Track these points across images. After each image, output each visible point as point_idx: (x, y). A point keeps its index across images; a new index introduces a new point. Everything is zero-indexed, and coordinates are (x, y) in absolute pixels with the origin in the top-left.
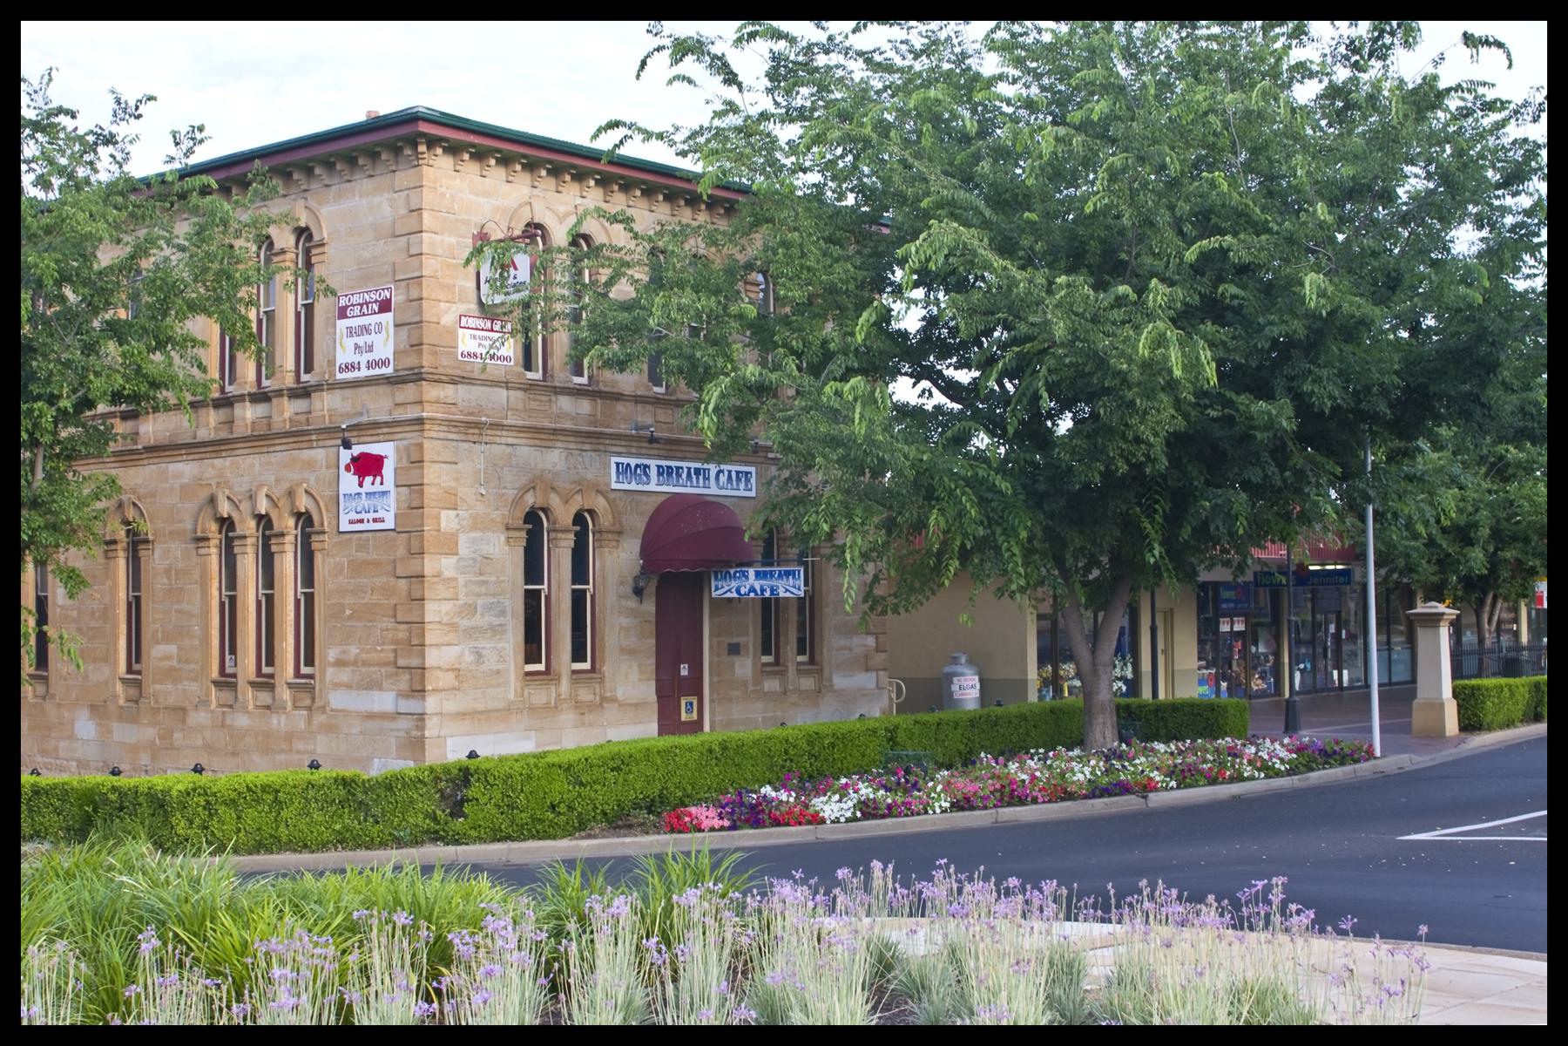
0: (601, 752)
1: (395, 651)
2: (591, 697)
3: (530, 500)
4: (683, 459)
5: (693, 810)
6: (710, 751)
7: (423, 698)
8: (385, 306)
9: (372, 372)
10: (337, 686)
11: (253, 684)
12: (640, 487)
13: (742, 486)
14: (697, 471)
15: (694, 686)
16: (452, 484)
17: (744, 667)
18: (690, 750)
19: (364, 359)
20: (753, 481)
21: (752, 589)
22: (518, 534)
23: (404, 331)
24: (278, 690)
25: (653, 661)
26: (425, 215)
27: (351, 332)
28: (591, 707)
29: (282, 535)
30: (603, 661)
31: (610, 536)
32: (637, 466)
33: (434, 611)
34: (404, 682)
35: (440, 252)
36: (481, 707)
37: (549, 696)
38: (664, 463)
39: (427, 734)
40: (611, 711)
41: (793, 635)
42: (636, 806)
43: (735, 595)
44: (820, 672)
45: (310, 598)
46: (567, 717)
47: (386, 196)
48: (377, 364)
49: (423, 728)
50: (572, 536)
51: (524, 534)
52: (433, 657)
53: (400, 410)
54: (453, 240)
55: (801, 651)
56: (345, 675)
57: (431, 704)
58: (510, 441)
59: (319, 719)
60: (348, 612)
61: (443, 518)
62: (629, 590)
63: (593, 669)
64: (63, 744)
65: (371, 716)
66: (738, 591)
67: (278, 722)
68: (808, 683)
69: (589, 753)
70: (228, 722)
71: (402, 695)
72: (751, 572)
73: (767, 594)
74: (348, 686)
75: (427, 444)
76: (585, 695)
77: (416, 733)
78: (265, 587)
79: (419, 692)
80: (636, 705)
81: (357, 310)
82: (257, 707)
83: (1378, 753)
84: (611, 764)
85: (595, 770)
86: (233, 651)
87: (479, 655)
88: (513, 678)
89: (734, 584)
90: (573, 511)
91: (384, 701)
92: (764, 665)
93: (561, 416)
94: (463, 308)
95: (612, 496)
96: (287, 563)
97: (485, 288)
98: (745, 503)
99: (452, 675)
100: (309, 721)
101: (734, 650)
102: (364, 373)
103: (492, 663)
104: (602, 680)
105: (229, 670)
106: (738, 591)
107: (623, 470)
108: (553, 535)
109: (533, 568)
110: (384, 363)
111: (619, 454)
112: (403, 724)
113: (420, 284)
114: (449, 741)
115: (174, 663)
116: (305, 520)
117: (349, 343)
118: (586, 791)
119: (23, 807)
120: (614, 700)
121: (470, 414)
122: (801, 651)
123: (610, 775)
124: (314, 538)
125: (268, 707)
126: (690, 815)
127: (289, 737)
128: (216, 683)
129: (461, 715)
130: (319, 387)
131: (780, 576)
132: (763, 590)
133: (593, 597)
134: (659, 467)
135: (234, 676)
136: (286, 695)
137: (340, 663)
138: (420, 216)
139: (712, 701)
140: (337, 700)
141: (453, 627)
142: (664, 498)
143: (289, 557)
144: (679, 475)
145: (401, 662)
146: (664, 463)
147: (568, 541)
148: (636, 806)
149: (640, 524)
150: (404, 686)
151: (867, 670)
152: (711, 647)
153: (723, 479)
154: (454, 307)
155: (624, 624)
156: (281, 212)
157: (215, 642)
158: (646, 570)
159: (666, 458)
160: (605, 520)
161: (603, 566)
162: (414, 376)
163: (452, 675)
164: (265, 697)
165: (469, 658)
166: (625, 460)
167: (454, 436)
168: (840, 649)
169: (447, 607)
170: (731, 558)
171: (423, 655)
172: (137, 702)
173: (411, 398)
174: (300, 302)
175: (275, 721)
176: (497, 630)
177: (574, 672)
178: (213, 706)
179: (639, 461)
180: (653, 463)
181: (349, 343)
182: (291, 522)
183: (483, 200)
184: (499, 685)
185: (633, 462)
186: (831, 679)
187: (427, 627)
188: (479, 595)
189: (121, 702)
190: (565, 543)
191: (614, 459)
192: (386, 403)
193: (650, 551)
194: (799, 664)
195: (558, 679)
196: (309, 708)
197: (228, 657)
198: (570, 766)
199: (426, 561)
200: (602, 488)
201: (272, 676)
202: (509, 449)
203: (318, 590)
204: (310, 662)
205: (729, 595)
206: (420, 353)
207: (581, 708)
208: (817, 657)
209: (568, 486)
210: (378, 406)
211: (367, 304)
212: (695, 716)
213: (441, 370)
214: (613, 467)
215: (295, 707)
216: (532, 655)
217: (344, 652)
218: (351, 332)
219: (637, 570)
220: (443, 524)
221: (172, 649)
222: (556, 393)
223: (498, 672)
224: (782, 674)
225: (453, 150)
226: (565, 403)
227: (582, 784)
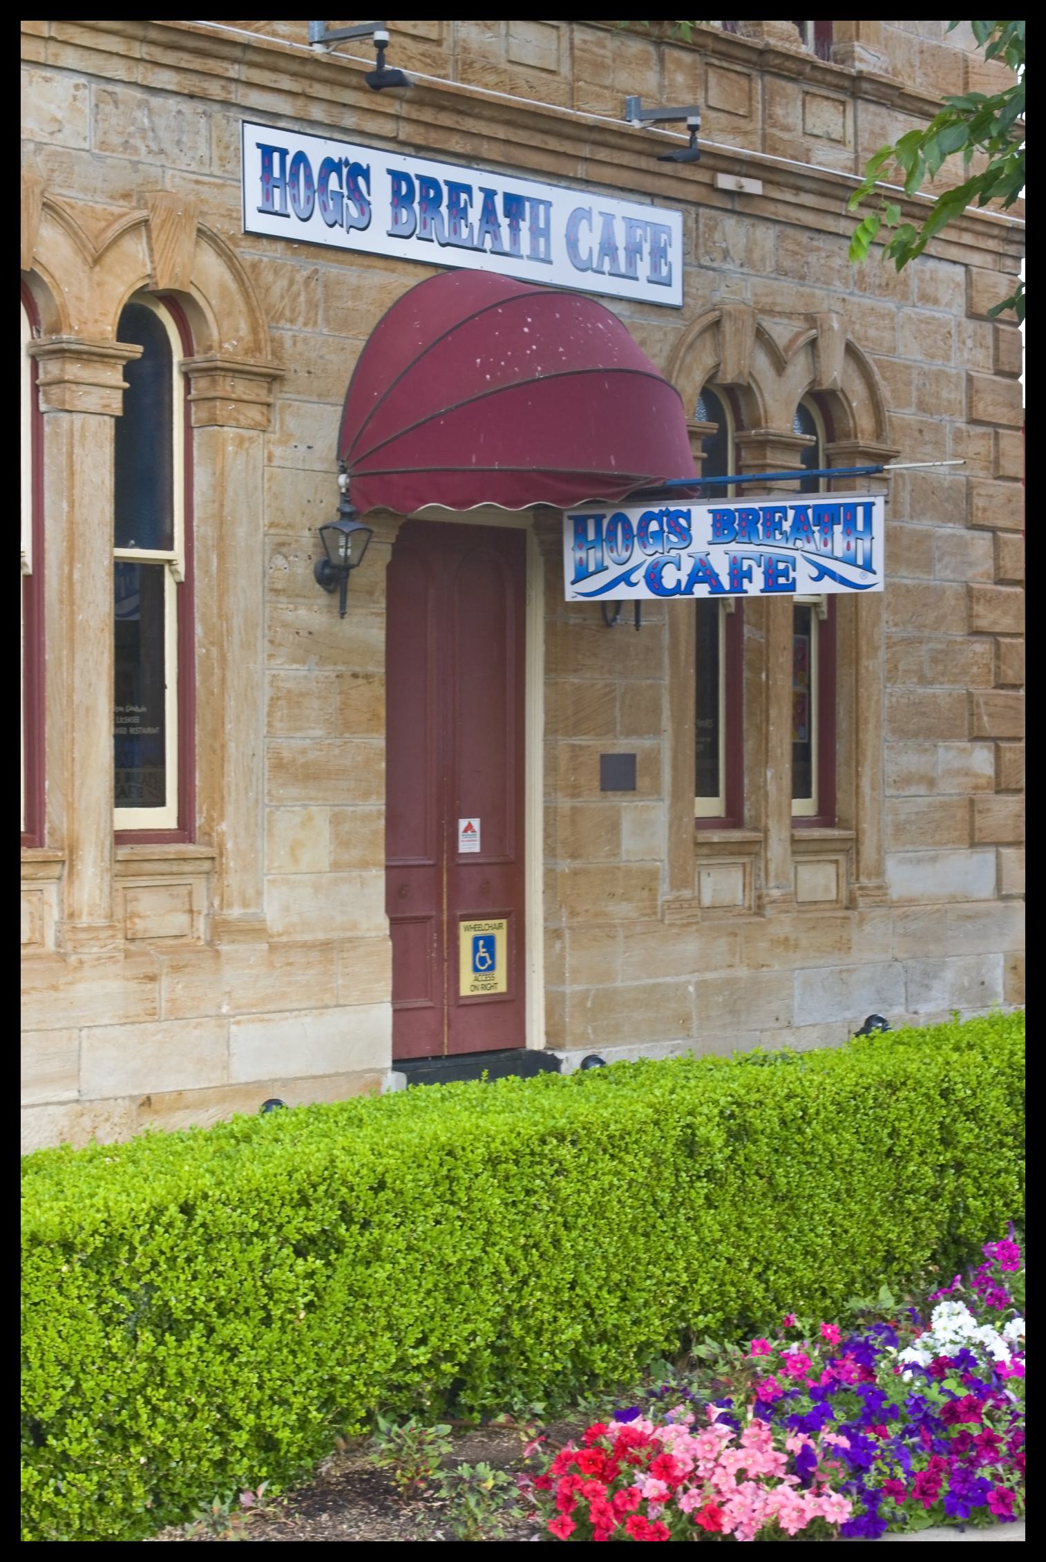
0: (253, 1172)
2: (179, 921)
4: (470, 160)
5: (676, 1440)
6: (690, 1146)
12: (337, 237)
13: (644, 268)
14: (514, 204)
15: (501, 889)
17: (647, 828)
18: (615, 1146)
21: (703, 572)
25: (377, 804)
28: (181, 955)
30: (218, 802)
31: (241, 388)
32: (330, 166)
38: (415, 166)
40: (243, 968)
41: (781, 738)
42: (400, 1405)
43: (642, 592)
44: (852, 848)
50: (115, 376)
55: (800, 789)
62: (304, 570)
63: (185, 830)
66: (654, 580)
68: (819, 880)
69: (195, 1176)
72: (701, 515)
76: (158, 913)
80: (326, 946)
84: (299, 1224)
85: (227, 1253)
89: (640, 556)
90: (119, 292)
92: (703, 823)
95: (248, 253)
98: (654, 320)
101: (620, 774)
104: (214, 865)
106: (654, 580)
107: (282, 170)
108: (51, 369)
111: (271, 119)
118: (185, 1354)
119: (745, 708)
120: (254, 931)
122: (800, 789)
123: (292, 1273)
126: (663, 1467)
131: (801, 526)
132: (739, 575)
133: (185, 590)
134: (398, 177)
139: (553, 934)
142: (409, 280)
144: (458, 212)
146: (415, 166)
147: (100, 393)
148: (400, 1405)
149: (328, 352)
151: (973, 844)
152: (551, 767)
158: (356, 507)
160: (226, 333)
161: (220, 485)
168: (906, 780)
170: (627, 489)
177: (122, 838)
179: (338, 151)
180: (380, 162)
185: (318, 150)
186: (879, 872)
190: (92, 399)
191: (256, 134)
193: (370, 444)
194: (797, 822)
198: (114, 1242)
200: (216, 224)
205: (621, 593)
208: (843, 806)
209: (102, 205)
212: (500, 981)
214: (254, 159)
219: (328, 507)
227: (166, 1323)
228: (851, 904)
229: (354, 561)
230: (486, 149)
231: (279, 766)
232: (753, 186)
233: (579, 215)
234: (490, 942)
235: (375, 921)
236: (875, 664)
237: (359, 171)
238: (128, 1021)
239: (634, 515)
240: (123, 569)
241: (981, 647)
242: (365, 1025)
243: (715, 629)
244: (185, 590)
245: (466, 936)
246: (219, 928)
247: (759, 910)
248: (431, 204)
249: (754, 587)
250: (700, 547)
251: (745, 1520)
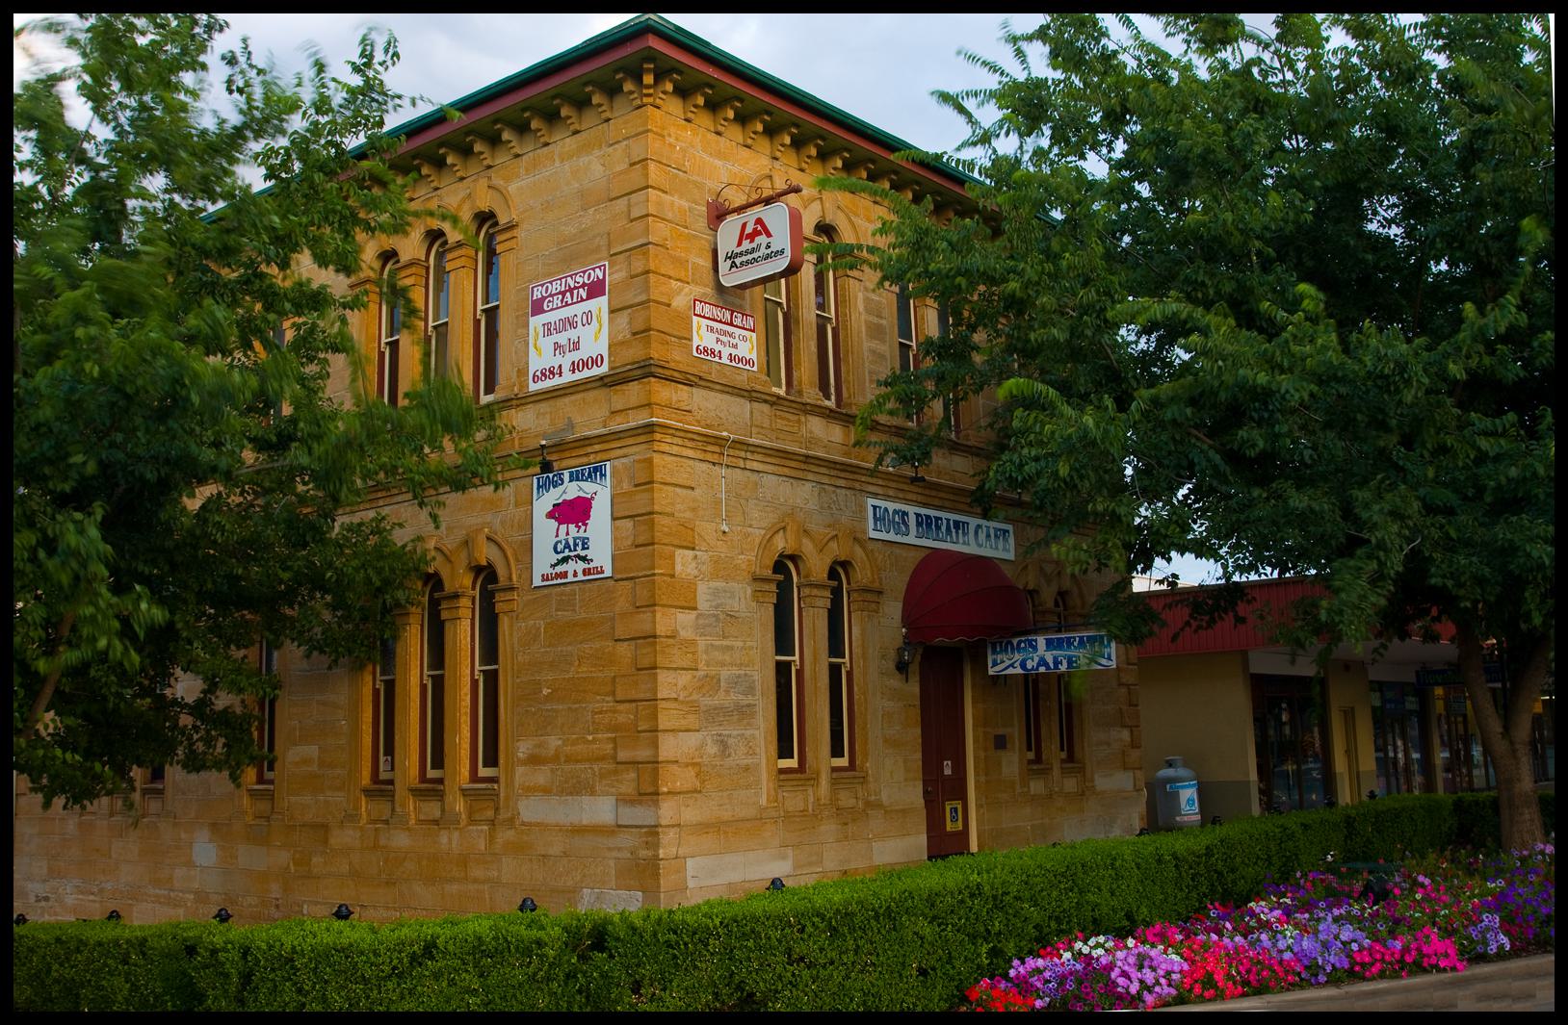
1: (614, 740)
3: (780, 544)
7: (656, 804)
8: (595, 290)
9: (578, 376)
10: (530, 791)
11: (414, 791)
12: (899, 539)
14: (957, 524)
16: (688, 515)
19: (565, 362)
20: (1011, 540)
21: (1043, 662)
22: (766, 587)
23: (623, 319)
24: (449, 798)
25: (919, 755)
26: (652, 166)
27: (549, 329)
29: (456, 596)
32: (895, 512)
33: (669, 684)
34: (628, 783)
35: (670, 216)
36: (726, 815)
37: (806, 801)
38: (924, 511)
39: (661, 853)
44: (1082, 770)
45: (492, 679)
46: (828, 828)
47: (597, 152)
48: (585, 364)
49: (656, 846)
51: (773, 587)
52: (670, 747)
53: (619, 418)
54: (685, 204)
55: (837, 752)
56: (541, 776)
57: (667, 811)
58: (756, 466)
59: (505, 835)
60: (545, 691)
61: (678, 560)
62: (892, 666)
64: (180, 872)
65: (579, 830)
66: (1023, 665)
67: (448, 841)
68: (1071, 784)
70: (382, 842)
71: (623, 800)
72: (1041, 641)
73: (1063, 668)
74: (546, 791)
75: (657, 459)
76: (846, 799)
77: (644, 853)
78: (431, 667)
79: (649, 795)
80: (903, 811)
81: (557, 301)
82: (420, 822)
83: (974, 847)
86: (390, 750)
87: (723, 744)
88: (764, 776)
89: (1018, 657)
90: (828, 561)
91: (600, 809)
93: (812, 441)
94: (697, 290)
95: (871, 546)
96: (463, 633)
97: (724, 266)
99: (691, 772)
100: (491, 838)
101: (1001, 743)
102: (568, 377)
103: (739, 757)
105: (383, 776)
106: (1023, 665)
108: (806, 591)
109: (783, 640)
110: (595, 362)
111: (875, 495)
112: (626, 840)
113: (646, 254)
114: (690, 862)
115: (315, 768)
116: (486, 574)
117: (546, 344)
120: (878, 805)
121: (708, 426)
122: (837, 752)
124: (499, 597)
125: (436, 822)
127: (464, 861)
128: (367, 792)
129: (704, 828)
130: (506, 403)
132: (1057, 663)
133: (849, 674)
134: (918, 515)
135: (391, 782)
136: (460, 806)
137: (534, 760)
138: (646, 168)
139: (979, 806)
140: (530, 810)
141: (694, 707)
142: (922, 554)
143: (466, 624)
144: (938, 528)
145: (622, 755)
146: (924, 511)
147: (824, 600)
149: (897, 582)
150: (627, 787)
152: (975, 741)
153: (982, 536)
154: (687, 288)
155: (887, 706)
156: (457, 195)
157: (367, 740)
158: (908, 641)
159: (925, 505)
162: (646, 371)
163: (691, 772)
164: (432, 809)
165: (712, 749)
166: (882, 504)
167: (690, 453)
169: (684, 678)
171: (655, 745)
172: (268, 819)
173: (634, 401)
174: (480, 307)
175: (444, 840)
176: (744, 713)
178: (363, 821)
180: (911, 510)
181: (546, 344)
182: (467, 580)
183: (719, 163)
184: (748, 787)
185: (891, 506)
187: (662, 705)
188: (723, 665)
189: (249, 819)
191: (871, 501)
192: (602, 412)
195: (815, 779)
196: (492, 822)
197: (382, 758)
199: (658, 615)
201: (441, 781)
202: (754, 477)
203: (504, 666)
204: (492, 760)
206: (648, 342)
207: (846, 817)
210: (589, 418)
211: (571, 290)
212: (960, 826)
213: (672, 365)
214: (870, 510)
215: (472, 821)
216: (785, 751)
217: (539, 746)
218: (549, 329)
219: (899, 642)
220: (678, 568)
221: (312, 751)
222: (806, 413)
223: (747, 769)
224: (1045, 772)
225: (683, 92)
226: (816, 425)
228: (1083, 794)
230: (947, 504)
231: (886, 741)
233: (979, 527)
235: (919, 801)
237: (905, 514)
238: (838, 841)
239: (1015, 642)
240: (778, 664)
241: (1124, 690)
242: (918, 842)
243: (1032, 685)
244: (849, 674)
247: (1050, 796)
248: (929, 525)
249: (1063, 668)
250: (1040, 654)
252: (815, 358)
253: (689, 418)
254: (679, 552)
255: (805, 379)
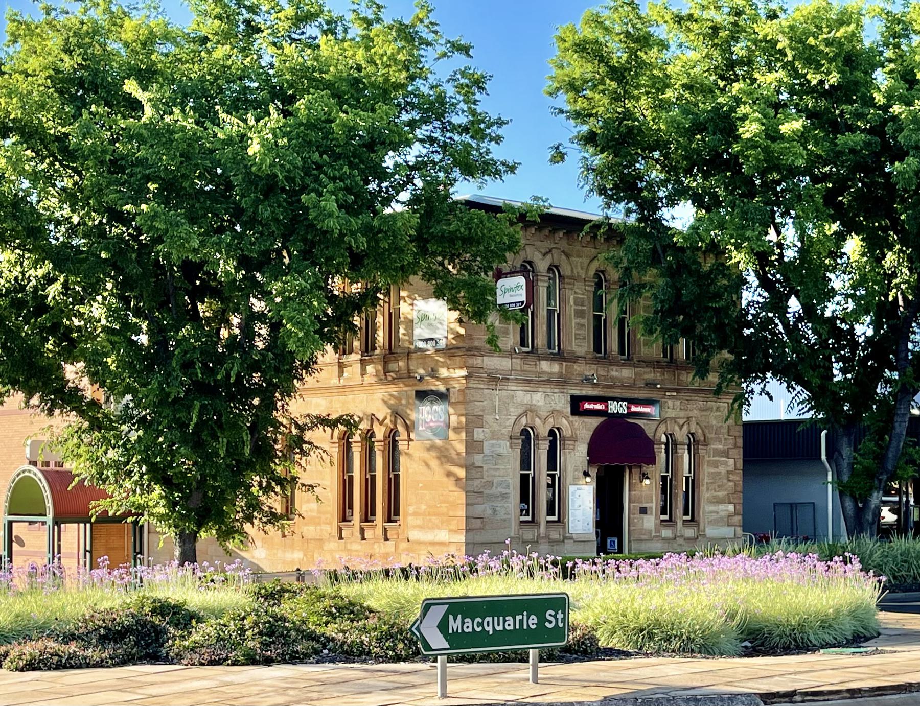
10: (414, 527)
51: (520, 441)
55: (686, 513)
56: (419, 521)
68: (690, 532)
92: (662, 521)
109: (525, 462)
115: (315, 514)
122: (686, 513)
133: (559, 478)
137: (415, 514)
145: (451, 514)
168: (711, 512)
177: (548, 522)
197: (347, 510)
208: (696, 518)
216: (663, 512)
220: (475, 436)
223: (505, 520)
229: (453, 400)
232: (675, 394)
234: (611, 545)
236: (703, 489)
245: (609, 541)
246: (565, 538)
251: (712, 7)
252: (545, 334)
253: (481, 371)
254: (476, 429)
255: (540, 344)
